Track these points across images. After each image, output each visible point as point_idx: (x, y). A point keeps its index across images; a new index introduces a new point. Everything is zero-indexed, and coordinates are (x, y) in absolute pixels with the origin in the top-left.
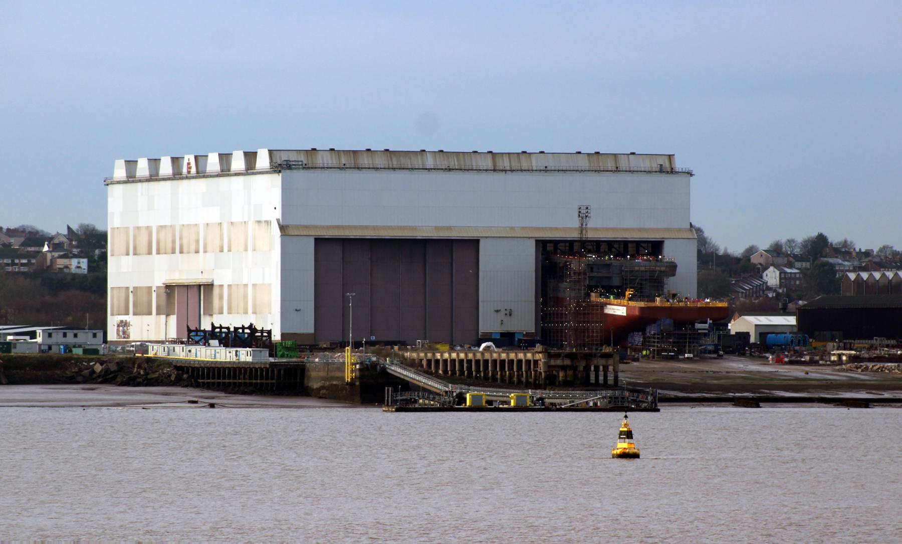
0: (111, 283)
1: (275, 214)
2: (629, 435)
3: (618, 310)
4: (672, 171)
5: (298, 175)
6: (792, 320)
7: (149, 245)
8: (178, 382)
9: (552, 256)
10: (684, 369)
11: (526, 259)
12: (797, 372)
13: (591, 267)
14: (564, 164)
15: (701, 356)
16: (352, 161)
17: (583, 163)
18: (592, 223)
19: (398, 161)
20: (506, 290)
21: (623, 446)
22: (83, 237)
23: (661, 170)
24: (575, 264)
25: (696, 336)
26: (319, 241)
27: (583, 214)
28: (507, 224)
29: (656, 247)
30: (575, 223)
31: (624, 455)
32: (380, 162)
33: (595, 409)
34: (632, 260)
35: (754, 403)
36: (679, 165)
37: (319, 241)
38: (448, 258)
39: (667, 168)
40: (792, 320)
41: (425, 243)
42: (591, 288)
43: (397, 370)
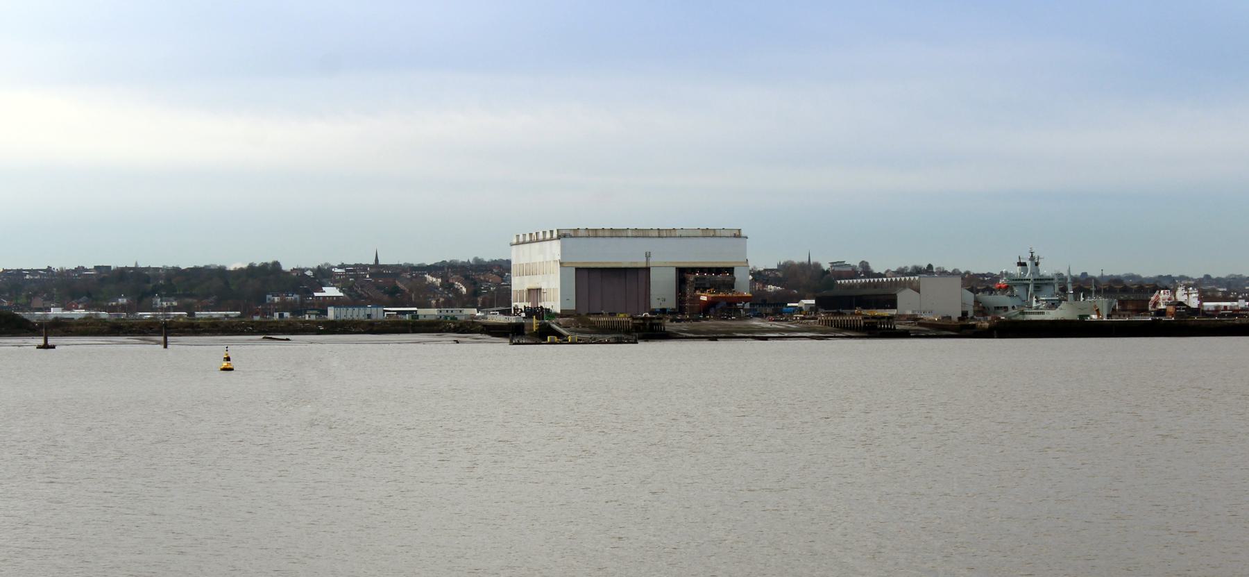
0: (513, 288)
1: (558, 258)
2: (228, 359)
3: (704, 298)
4: (739, 236)
5: (568, 240)
6: (813, 302)
7: (529, 271)
8: (481, 332)
9: (682, 273)
10: (733, 323)
11: (672, 275)
12: (776, 325)
13: (696, 279)
14: (691, 234)
15: (740, 318)
16: (594, 234)
17: (700, 233)
18: (651, 260)
19: (615, 233)
20: (662, 291)
21: (225, 364)
22: (860, 270)
23: (735, 236)
24: (691, 278)
25: (738, 310)
26: (577, 269)
27: (648, 256)
28: (663, 263)
29: (730, 270)
30: (644, 260)
31: (225, 369)
32: (607, 234)
33: (608, 343)
34: (720, 276)
35: (715, 339)
36: (743, 233)
37: (577, 269)
38: (638, 275)
39: (738, 235)
40: (813, 302)
41: (626, 269)
42: (696, 289)
43: (555, 326)
